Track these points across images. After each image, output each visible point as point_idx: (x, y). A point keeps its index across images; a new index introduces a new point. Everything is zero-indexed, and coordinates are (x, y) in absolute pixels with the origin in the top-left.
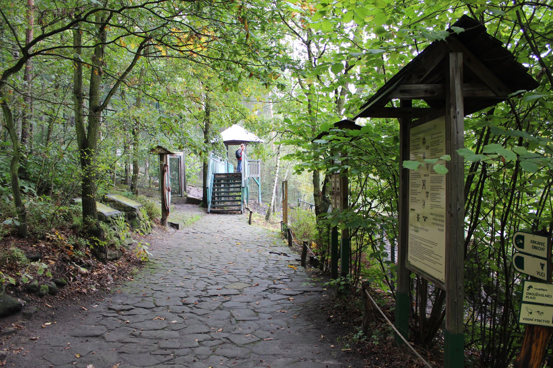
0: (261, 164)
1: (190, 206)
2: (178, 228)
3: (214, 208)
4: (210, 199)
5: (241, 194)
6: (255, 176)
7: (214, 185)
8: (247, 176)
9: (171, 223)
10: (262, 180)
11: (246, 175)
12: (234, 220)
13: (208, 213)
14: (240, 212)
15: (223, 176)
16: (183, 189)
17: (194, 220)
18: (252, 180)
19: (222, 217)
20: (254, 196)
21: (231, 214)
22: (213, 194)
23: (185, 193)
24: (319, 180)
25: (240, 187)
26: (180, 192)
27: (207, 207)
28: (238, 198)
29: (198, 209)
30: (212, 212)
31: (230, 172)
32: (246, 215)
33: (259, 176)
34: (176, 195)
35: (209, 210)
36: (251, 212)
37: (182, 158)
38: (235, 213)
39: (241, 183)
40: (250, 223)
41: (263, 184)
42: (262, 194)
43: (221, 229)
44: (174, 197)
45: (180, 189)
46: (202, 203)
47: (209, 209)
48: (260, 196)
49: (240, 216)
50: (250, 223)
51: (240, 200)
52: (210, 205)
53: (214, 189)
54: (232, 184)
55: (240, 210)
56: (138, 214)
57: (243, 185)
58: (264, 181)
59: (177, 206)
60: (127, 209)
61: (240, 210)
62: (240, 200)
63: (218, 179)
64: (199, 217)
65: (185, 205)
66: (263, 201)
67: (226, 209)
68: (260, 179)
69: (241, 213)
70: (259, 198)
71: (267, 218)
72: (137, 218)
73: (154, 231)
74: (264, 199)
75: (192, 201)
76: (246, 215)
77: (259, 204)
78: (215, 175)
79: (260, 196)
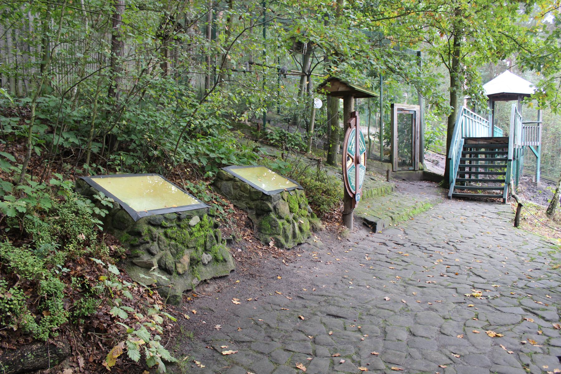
0: (543, 129)
1: (425, 184)
2: (374, 230)
3: (462, 189)
4: (454, 176)
5: (506, 170)
6: (532, 144)
7: (464, 155)
8: (519, 143)
9: (365, 220)
10: (542, 150)
11: (517, 141)
12: (488, 214)
13: (449, 198)
14: (502, 200)
15: (481, 142)
16: (417, 160)
17: (416, 212)
18: (528, 150)
19: (469, 206)
20: (530, 172)
21: (486, 201)
22: (462, 168)
23: (420, 165)
24: (257, 170)
25: (506, 160)
26: (413, 163)
27: (448, 188)
28: (500, 177)
29: (435, 190)
30: (456, 197)
31: (496, 135)
32: (511, 206)
33: (539, 144)
34: (406, 168)
35: (450, 194)
36: (520, 205)
37: (418, 114)
38: (493, 201)
39: (507, 153)
40: (516, 225)
41: (544, 155)
42: (541, 168)
43: (456, 235)
44: (403, 170)
45: (413, 158)
46: (441, 182)
47: (451, 191)
48: (539, 173)
49: (501, 207)
50: (516, 225)
51: (503, 181)
52: (453, 185)
53: (462, 161)
54: (498, 154)
55: (502, 197)
56: (275, 208)
57: (511, 156)
58: (546, 152)
59: (403, 185)
60: (255, 197)
61: (502, 197)
62: (503, 181)
63: (472, 145)
64: (429, 206)
65: (419, 183)
66: (542, 179)
67: (480, 193)
68: (540, 148)
69: (504, 202)
70: (536, 175)
71: (550, 212)
72: (273, 215)
73: (316, 238)
74: (544, 176)
75: (429, 177)
76: (511, 206)
77: (535, 184)
78: (467, 139)
79: (539, 173)
